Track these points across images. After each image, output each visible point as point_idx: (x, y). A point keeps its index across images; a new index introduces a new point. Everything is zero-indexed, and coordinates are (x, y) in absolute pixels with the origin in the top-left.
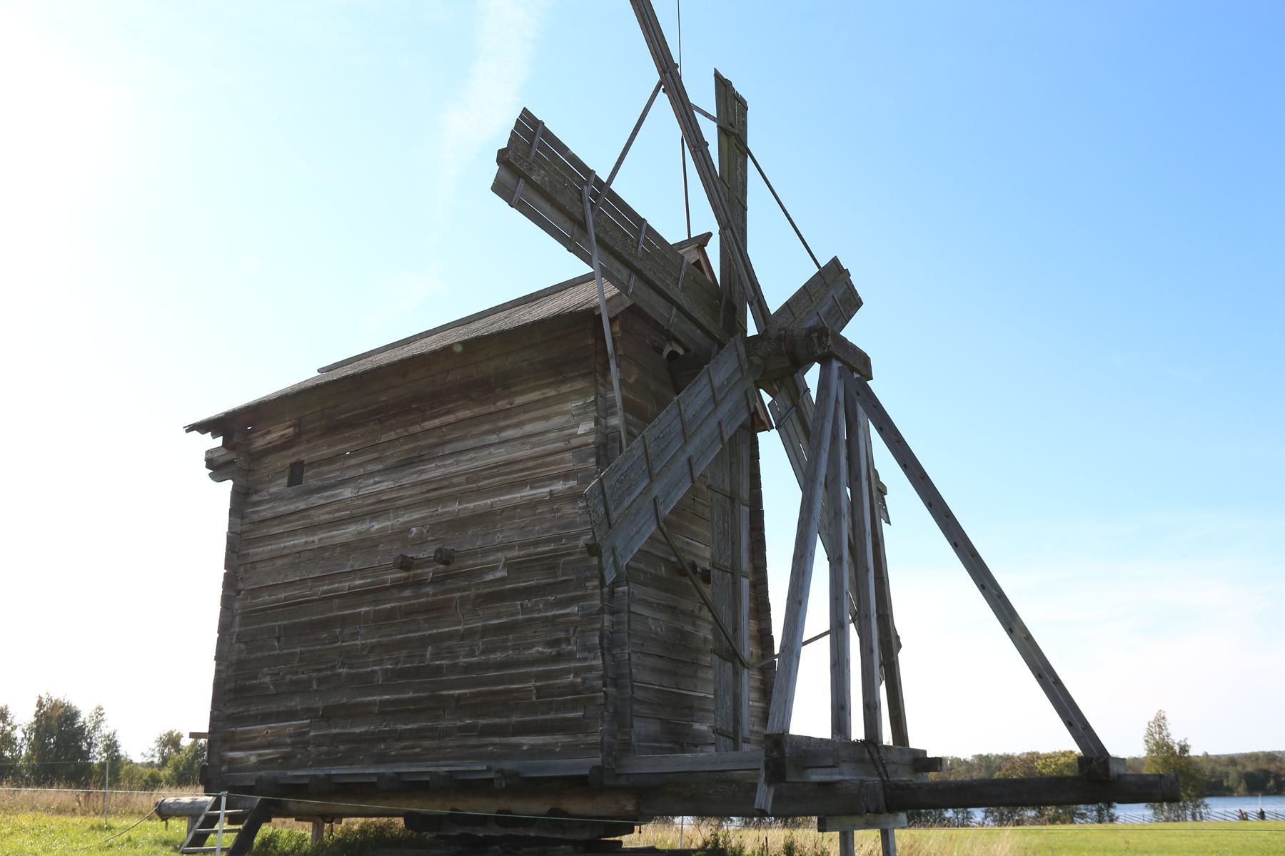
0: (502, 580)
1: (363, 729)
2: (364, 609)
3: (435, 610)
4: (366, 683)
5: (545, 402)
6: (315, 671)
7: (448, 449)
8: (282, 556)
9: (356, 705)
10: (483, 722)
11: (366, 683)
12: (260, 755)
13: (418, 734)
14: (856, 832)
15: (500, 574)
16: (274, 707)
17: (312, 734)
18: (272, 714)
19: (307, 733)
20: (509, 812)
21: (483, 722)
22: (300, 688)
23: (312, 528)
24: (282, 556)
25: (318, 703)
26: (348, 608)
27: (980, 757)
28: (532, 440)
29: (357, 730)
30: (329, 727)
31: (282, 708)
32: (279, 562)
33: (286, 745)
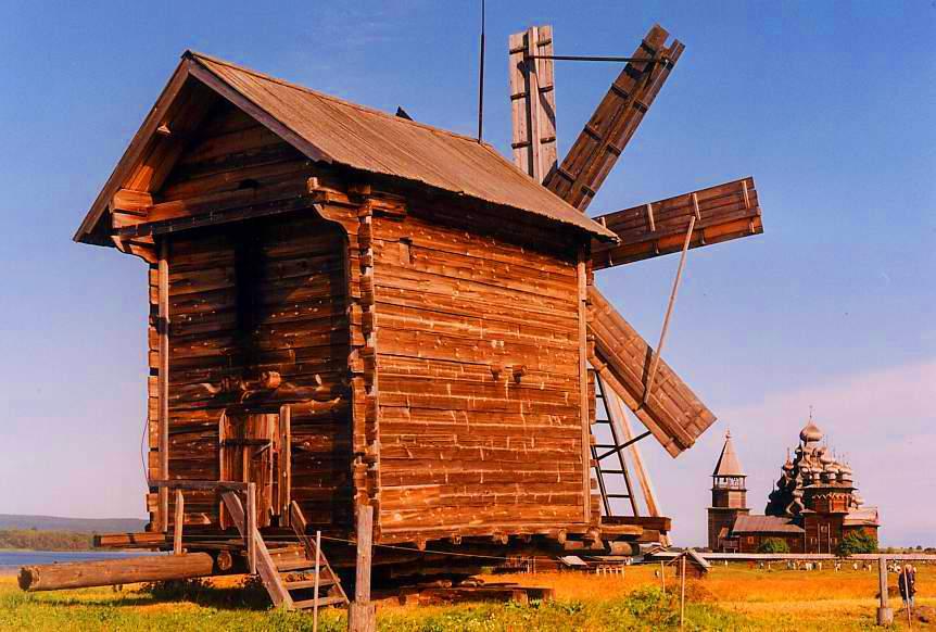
2: (469, 398)
16: (414, 471)
26: (458, 393)
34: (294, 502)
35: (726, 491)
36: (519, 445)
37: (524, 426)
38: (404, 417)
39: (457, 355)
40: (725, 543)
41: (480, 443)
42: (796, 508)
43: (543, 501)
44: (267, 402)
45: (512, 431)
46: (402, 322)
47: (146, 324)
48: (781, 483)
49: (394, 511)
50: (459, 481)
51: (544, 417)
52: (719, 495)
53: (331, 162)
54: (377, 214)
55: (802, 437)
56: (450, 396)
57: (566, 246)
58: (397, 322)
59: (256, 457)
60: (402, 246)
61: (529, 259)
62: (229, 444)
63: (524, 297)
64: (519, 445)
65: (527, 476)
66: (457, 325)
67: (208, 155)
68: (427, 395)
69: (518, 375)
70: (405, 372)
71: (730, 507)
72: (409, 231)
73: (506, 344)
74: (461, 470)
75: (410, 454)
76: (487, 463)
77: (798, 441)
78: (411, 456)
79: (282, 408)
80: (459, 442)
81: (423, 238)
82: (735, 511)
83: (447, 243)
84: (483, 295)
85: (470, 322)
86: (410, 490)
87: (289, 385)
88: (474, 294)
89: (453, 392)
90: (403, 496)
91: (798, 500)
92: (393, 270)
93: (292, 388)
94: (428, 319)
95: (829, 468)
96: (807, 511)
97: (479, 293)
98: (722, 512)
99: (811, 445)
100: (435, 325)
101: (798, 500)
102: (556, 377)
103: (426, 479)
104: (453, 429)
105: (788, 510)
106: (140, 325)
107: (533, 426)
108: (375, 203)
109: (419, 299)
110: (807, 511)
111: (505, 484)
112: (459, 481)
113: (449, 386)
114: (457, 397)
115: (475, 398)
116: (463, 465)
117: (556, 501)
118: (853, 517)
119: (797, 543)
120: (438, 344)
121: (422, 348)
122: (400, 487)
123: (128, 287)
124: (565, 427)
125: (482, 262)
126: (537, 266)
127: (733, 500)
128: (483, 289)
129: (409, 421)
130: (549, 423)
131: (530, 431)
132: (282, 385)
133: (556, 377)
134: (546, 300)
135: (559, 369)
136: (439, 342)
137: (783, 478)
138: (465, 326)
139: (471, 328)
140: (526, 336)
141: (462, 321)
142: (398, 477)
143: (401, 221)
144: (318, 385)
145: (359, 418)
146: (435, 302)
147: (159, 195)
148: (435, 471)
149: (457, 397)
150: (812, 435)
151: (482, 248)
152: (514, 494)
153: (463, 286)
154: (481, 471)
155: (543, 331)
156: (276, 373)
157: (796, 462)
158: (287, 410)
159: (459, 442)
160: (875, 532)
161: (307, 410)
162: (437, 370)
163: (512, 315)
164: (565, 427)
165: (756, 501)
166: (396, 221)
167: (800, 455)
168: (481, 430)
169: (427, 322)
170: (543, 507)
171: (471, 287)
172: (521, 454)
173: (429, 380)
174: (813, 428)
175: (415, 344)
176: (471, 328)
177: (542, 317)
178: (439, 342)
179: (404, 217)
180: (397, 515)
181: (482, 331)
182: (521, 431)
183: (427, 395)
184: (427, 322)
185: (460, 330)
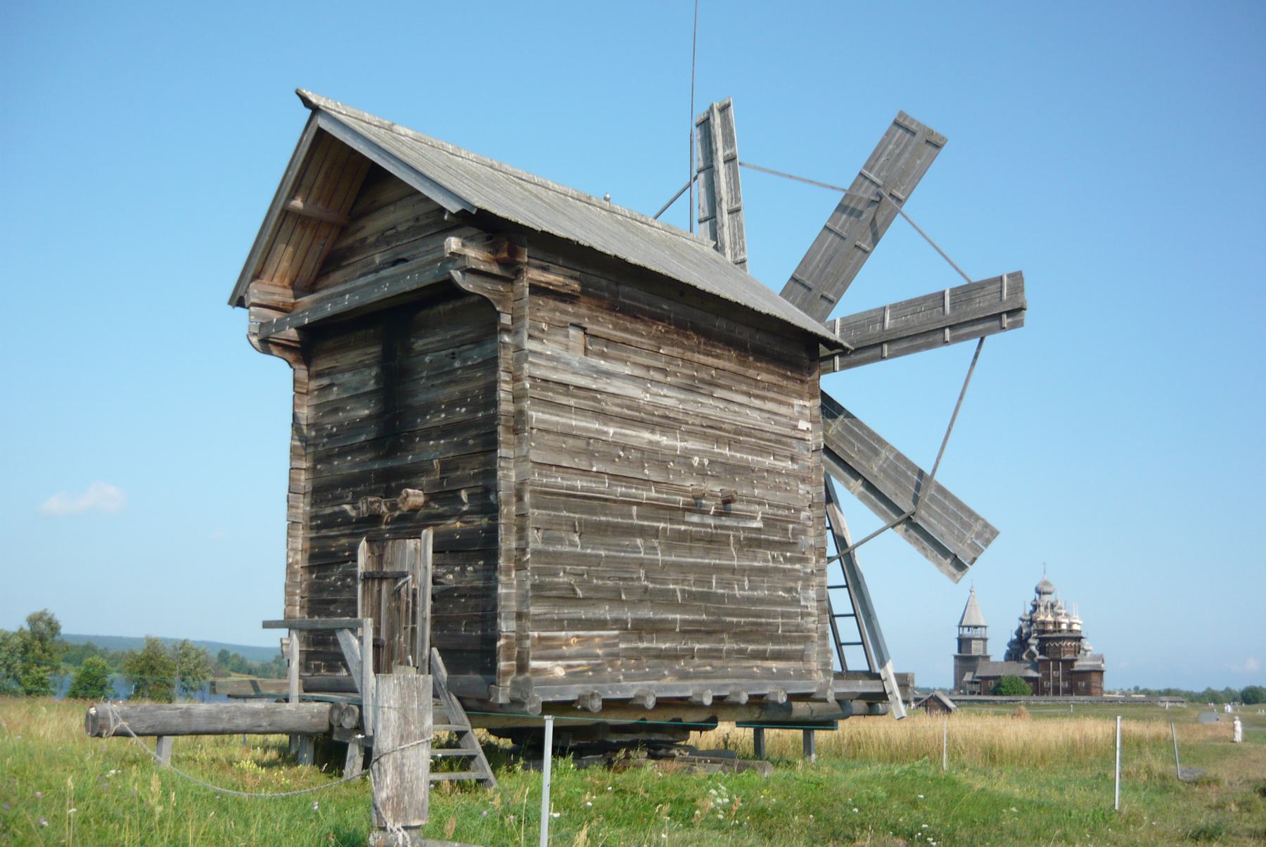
0: (758, 530)
1: (668, 645)
2: (662, 525)
3: (713, 541)
4: (666, 600)
5: (771, 386)
6: (620, 579)
7: (719, 393)
8: (575, 436)
9: (662, 621)
10: (751, 647)
11: (666, 600)
12: (569, 667)
13: (705, 654)
14: (766, 731)
15: (757, 524)
16: (583, 613)
17: (622, 646)
18: (580, 620)
19: (616, 645)
20: (680, 720)
21: (751, 647)
22: (614, 598)
23: (601, 415)
24: (575, 436)
25: (628, 615)
26: (647, 518)
27: (1228, 689)
28: (777, 418)
29: (663, 646)
30: (641, 639)
31: (590, 615)
32: (571, 441)
33: (597, 656)
34: (435, 650)
35: (970, 640)
36: (729, 585)
37: (735, 563)
38: (573, 544)
39: (646, 471)
40: (968, 686)
41: (676, 582)
42: (1032, 655)
43: (761, 656)
44: (409, 525)
45: (718, 569)
46: (571, 426)
47: (288, 431)
48: (1019, 632)
49: (559, 665)
50: (642, 628)
51: (761, 552)
52: (963, 642)
53: (474, 212)
54: (538, 290)
55: (1039, 592)
56: (636, 522)
57: (791, 351)
58: (564, 425)
59: (396, 594)
60: (572, 331)
61: (743, 363)
62: (368, 577)
63: (736, 408)
64: (729, 585)
65: (738, 624)
66: (647, 435)
67: (360, 235)
68: (603, 518)
69: (727, 501)
70: (574, 488)
71: (974, 653)
72: (583, 317)
73: (711, 462)
74: (651, 615)
75: (579, 591)
76: (682, 607)
77: (1032, 595)
78: (580, 593)
79: (424, 531)
80: (647, 578)
81: (605, 326)
82: (975, 658)
83: (639, 333)
84: (681, 401)
85: (663, 433)
86: (578, 637)
87: (432, 504)
88: (671, 399)
89: (639, 517)
90: (567, 645)
91: (1033, 648)
92: (552, 352)
93: (436, 508)
94: (605, 424)
95: (1061, 619)
96: (1042, 657)
97: (678, 399)
98: (966, 658)
99: (1046, 598)
100: (615, 433)
101: (1033, 648)
102: (778, 507)
103: (601, 624)
104: (641, 563)
105: (1024, 657)
106: (284, 438)
107: (746, 563)
108: (535, 275)
109: (595, 400)
110: (1042, 657)
111: (709, 633)
112: (642, 628)
113: (635, 508)
114: (646, 523)
115: (669, 526)
116: (652, 609)
117: (777, 656)
118: (1082, 664)
119: (1037, 687)
120: (619, 457)
121: (597, 459)
122: (563, 633)
123: (269, 396)
124: (789, 566)
125: (680, 363)
126: (751, 372)
127: (976, 648)
128: (682, 396)
129: (579, 550)
130: (767, 561)
131: (743, 570)
132: (426, 504)
133: (778, 507)
134: (767, 415)
135: (778, 497)
136: (621, 453)
137: (1020, 630)
138: (656, 437)
139: (665, 440)
140: (738, 455)
141: (653, 432)
142: (561, 620)
143: (571, 303)
144: (464, 504)
145: (508, 542)
146: (618, 405)
147: (303, 286)
148: (615, 614)
149: (646, 523)
150: (1046, 589)
151: (681, 346)
152: (720, 646)
153: (655, 390)
154: (678, 616)
155: (762, 451)
156: (417, 491)
157: (1032, 613)
158: (428, 534)
159: (647, 578)
160: (1102, 679)
161: (452, 533)
162: (619, 489)
163: (720, 429)
164: (789, 566)
165: (997, 650)
166: (564, 301)
167: (1036, 607)
168: (680, 567)
169: (605, 429)
170: (759, 663)
171: (665, 391)
172: (733, 598)
173: (606, 500)
174: (1046, 583)
175: (591, 455)
176: (665, 440)
177: (758, 434)
178: (621, 453)
179: (576, 297)
180: (265, 724)
181: (679, 444)
182: (733, 570)
183: (603, 518)
184: (605, 429)
185: (650, 442)
